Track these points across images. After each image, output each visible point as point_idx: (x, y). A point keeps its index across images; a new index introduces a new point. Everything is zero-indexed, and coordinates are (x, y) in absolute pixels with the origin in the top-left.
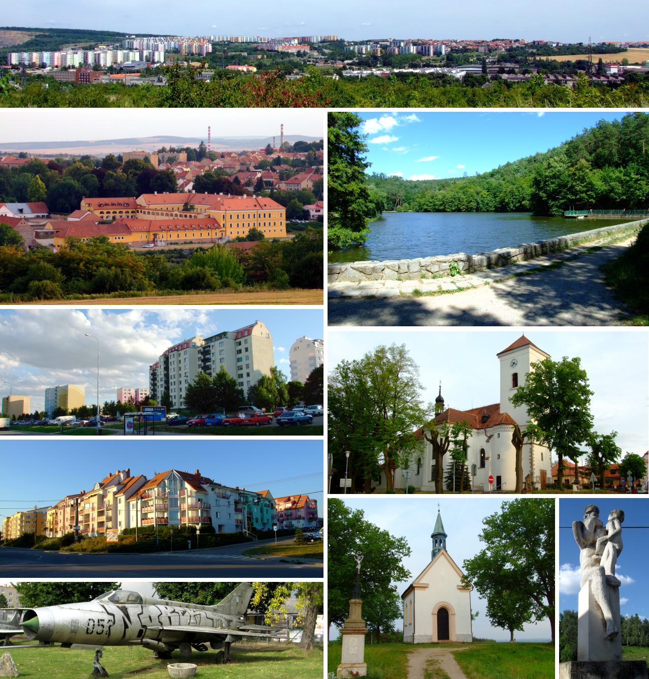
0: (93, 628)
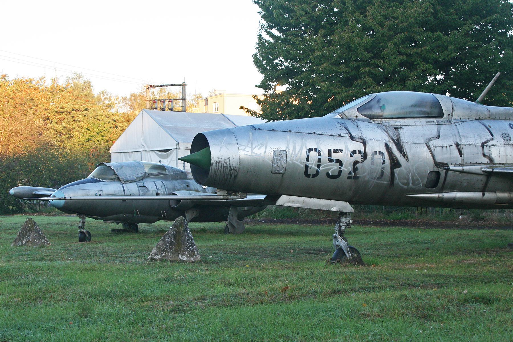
0: (319, 166)
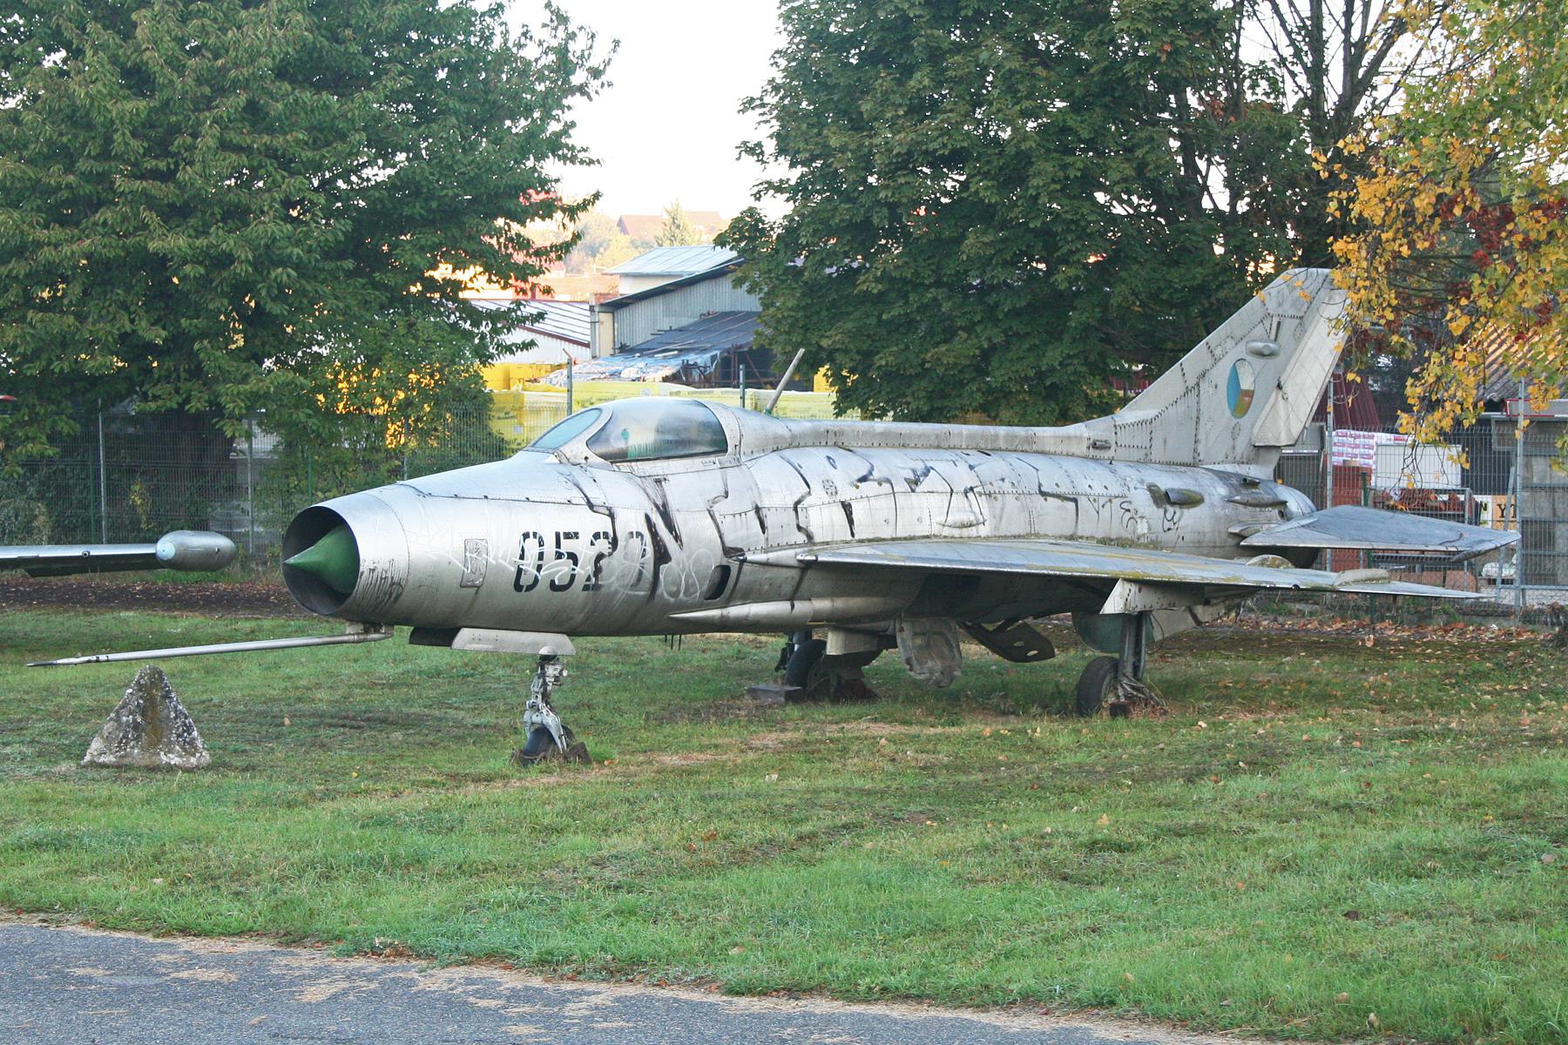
0: (539, 568)
